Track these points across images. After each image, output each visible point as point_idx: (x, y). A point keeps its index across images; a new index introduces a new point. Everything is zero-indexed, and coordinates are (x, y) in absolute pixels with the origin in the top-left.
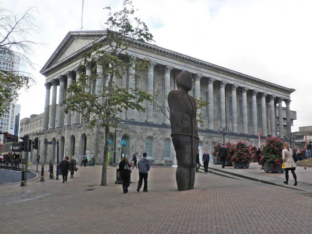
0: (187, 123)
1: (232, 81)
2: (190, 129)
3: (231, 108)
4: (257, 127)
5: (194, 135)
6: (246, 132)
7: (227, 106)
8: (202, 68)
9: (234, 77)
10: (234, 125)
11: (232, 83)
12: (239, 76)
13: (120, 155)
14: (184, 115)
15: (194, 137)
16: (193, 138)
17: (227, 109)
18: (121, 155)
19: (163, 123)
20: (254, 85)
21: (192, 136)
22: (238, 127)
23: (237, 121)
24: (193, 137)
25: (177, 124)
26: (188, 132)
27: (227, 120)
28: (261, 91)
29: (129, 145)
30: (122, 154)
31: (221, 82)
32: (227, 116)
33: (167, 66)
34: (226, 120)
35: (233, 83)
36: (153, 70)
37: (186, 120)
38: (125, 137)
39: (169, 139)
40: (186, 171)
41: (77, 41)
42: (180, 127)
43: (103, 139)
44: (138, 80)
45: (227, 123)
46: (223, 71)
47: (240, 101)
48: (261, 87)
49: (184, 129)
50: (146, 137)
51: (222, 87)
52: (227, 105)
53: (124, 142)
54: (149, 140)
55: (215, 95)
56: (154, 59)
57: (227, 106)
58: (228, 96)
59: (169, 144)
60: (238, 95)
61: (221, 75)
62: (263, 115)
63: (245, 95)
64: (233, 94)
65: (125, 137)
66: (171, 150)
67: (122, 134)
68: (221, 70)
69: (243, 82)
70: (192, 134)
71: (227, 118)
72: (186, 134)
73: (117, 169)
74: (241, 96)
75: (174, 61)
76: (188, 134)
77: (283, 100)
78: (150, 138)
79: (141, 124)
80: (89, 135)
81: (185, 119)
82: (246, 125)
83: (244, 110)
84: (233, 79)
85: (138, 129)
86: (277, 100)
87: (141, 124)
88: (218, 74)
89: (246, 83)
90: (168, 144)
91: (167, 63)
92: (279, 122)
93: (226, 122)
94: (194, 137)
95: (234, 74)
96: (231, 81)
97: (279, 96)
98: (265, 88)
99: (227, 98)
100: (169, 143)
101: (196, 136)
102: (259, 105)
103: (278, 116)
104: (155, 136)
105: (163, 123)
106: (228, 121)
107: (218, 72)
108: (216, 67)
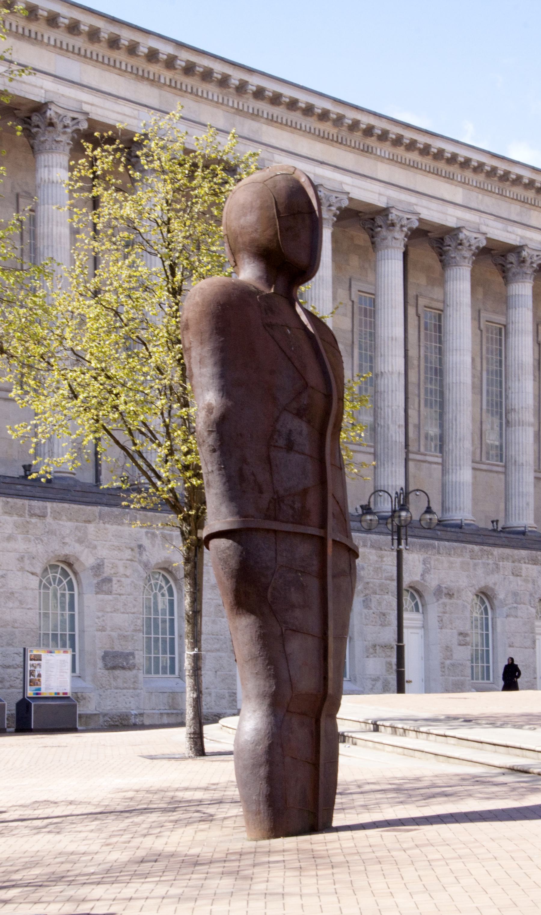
1: (451, 210)
2: (312, 501)
3: (438, 372)
5: (333, 534)
8: (272, 121)
9: (464, 183)
10: (451, 478)
11: (449, 217)
14: (277, 420)
15: (334, 541)
17: (413, 378)
21: (323, 540)
22: (475, 484)
23: (474, 453)
24: (330, 543)
25: (241, 469)
26: (301, 517)
27: (413, 447)
33: (46, 104)
34: (407, 445)
35: (451, 222)
37: (290, 447)
39: (70, 565)
41: (475, 319)
42: (261, 492)
44: (525, 380)
45: (411, 464)
49: (278, 500)
51: (389, 241)
52: (413, 352)
55: (342, 293)
57: (416, 362)
58: (422, 302)
59: (67, 592)
60: (480, 296)
61: (384, 171)
66: (82, 631)
69: (514, 211)
70: (323, 525)
71: (411, 434)
74: (505, 302)
75: (92, 75)
76: (301, 529)
81: (281, 442)
83: (514, 385)
84: (456, 193)
88: (365, 164)
90: (63, 595)
91: (48, 84)
93: (407, 460)
94: (334, 541)
96: (443, 203)
99: (411, 311)
100: (71, 588)
101: (344, 540)
106: (418, 452)
107: (366, 151)
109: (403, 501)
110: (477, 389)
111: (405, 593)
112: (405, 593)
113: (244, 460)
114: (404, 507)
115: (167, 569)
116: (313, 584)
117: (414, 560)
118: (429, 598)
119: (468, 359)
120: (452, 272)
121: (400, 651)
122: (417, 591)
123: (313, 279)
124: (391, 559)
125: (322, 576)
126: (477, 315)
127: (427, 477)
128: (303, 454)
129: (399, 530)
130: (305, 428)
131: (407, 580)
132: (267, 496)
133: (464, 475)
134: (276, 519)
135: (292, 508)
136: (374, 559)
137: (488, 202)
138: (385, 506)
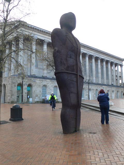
0: (71, 61)
1: (92, 54)
4: (106, 80)
6: (100, 82)
7: (89, 68)
11: (92, 54)
12: (96, 50)
13: (27, 96)
16: (78, 77)
18: (27, 97)
19: (53, 77)
20: (104, 56)
21: (77, 75)
22: (96, 79)
24: (78, 75)
25: (61, 61)
26: (73, 70)
28: (108, 59)
29: (32, 90)
30: (27, 96)
31: (86, 53)
32: (90, 73)
35: (93, 55)
36: (46, 45)
37: (70, 57)
38: (30, 86)
40: (70, 112)
43: (15, 86)
46: (87, 47)
47: (97, 66)
48: (108, 57)
49: (68, 67)
50: (42, 85)
52: (89, 67)
53: (29, 88)
54: (44, 88)
56: (47, 39)
61: (86, 50)
62: (109, 73)
63: (99, 61)
64: (93, 60)
65: (30, 86)
67: (28, 84)
68: (86, 47)
69: (98, 54)
70: (77, 72)
72: (70, 72)
73: (11, 108)
76: (73, 72)
77: (119, 65)
78: (45, 86)
79: (40, 78)
80: (7, 85)
82: (100, 79)
83: (99, 70)
84: (93, 52)
85: (38, 81)
86: (116, 65)
87: (40, 78)
88: (85, 49)
89: (100, 55)
92: (117, 78)
95: (94, 49)
96: (92, 53)
97: (117, 62)
98: (110, 58)
102: (107, 68)
103: (116, 75)
104: (48, 85)
105: (53, 77)
108: (84, 45)
109: (89, 80)
110: (95, 70)
111: (89, 90)
112: (89, 90)
113: (61, 59)
114: (89, 81)
115: (56, 86)
116: (76, 83)
117: (90, 86)
118: (91, 90)
119: (94, 67)
120: (93, 59)
121: (89, 95)
122: (90, 89)
123: (75, 29)
124: (88, 87)
125: (77, 82)
126: (95, 64)
127: (91, 78)
128: (73, 59)
129: (89, 83)
130: (73, 54)
131: (89, 88)
132: (66, 66)
133: (94, 78)
134: (68, 70)
135: (71, 69)
136: (85, 86)
137: (96, 53)
138: (87, 81)
